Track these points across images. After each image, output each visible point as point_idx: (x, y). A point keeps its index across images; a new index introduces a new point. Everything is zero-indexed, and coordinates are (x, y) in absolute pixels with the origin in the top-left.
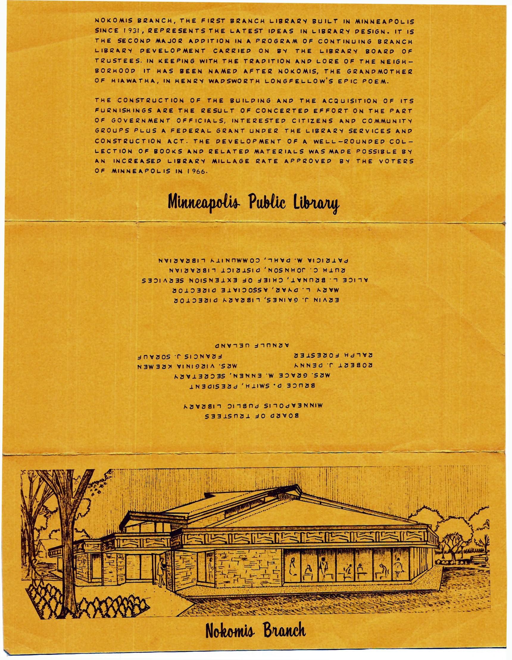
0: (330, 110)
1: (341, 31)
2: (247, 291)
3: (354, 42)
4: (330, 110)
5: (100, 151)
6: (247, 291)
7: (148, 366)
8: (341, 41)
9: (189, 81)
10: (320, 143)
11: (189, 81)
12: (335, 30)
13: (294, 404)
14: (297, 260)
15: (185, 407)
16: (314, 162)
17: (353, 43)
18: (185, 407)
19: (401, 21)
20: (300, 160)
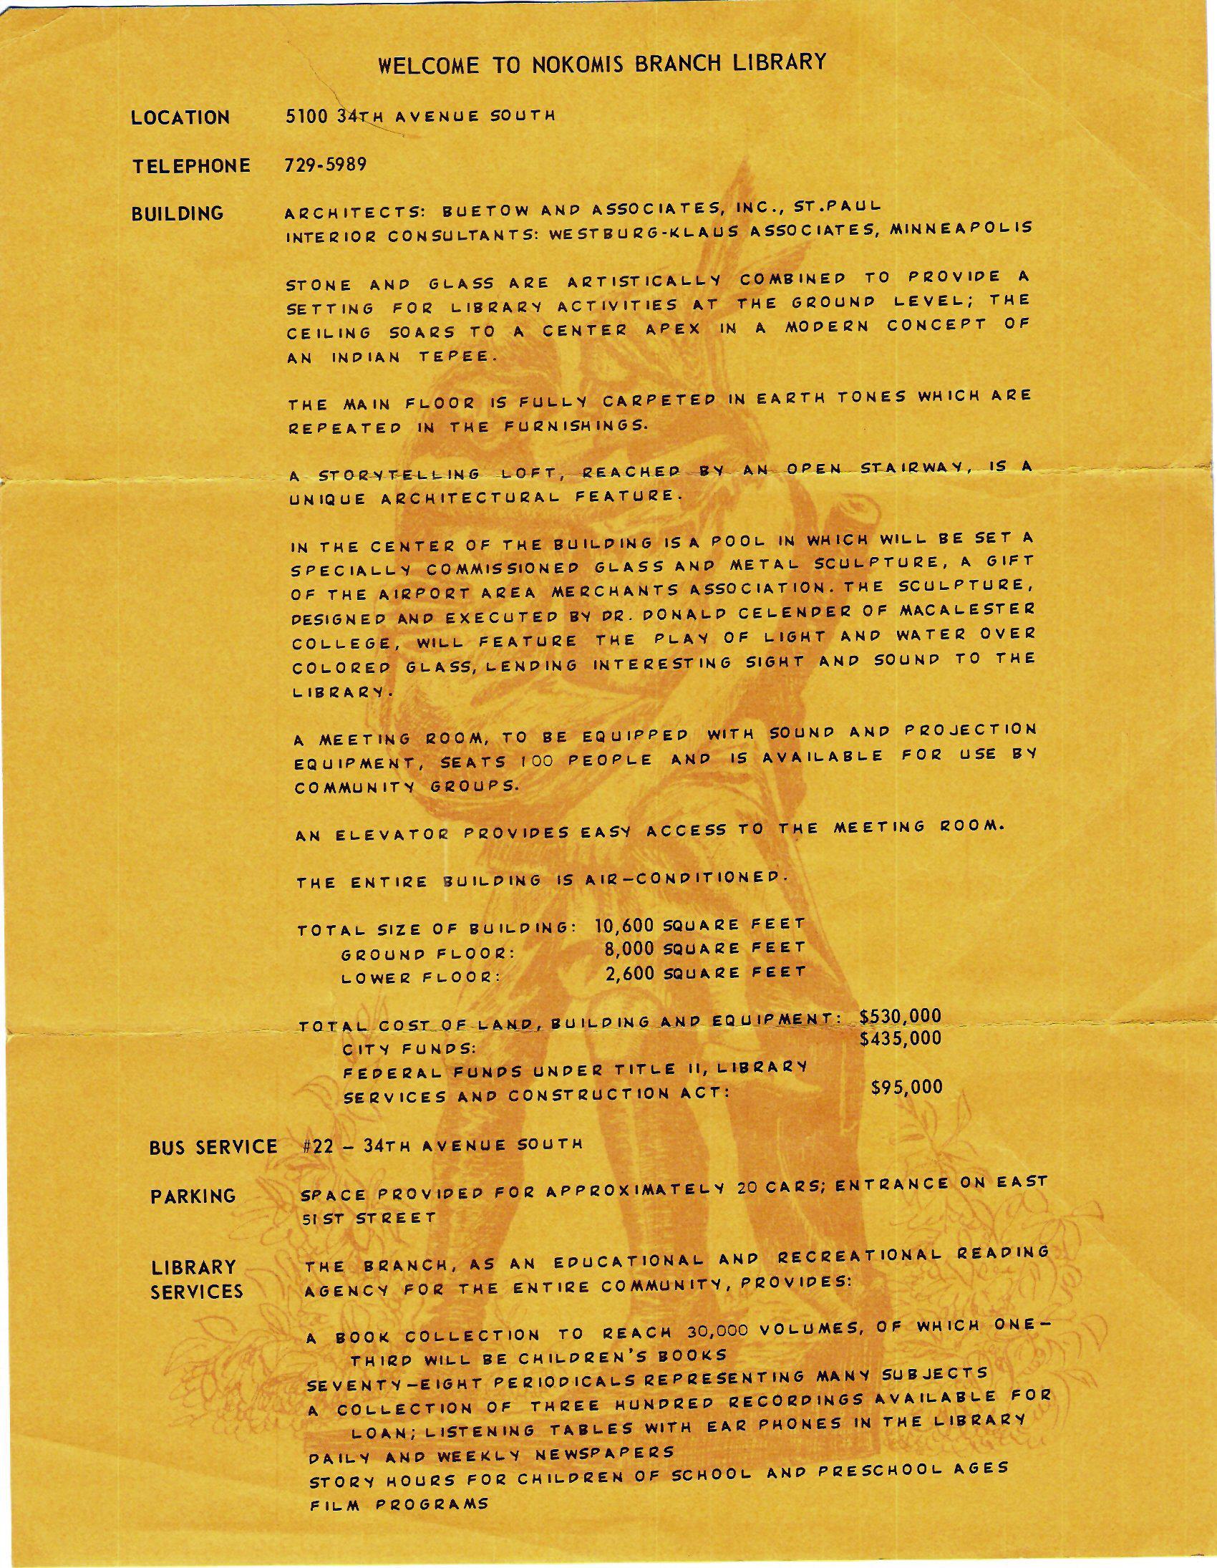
0: (404, 307)
1: (799, 1185)
2: (799, 229)
3: (345, 500)
4: (404, 307)
5: (462, 1337)
6: (799, 229)
7: (744, 567)
8: (768, 1377)
9: (922, 326)
10: (388, 982)
11: (922, 326)
12: (453, 1501)
13: (944, 614)
14: (998, 826)
15: (370, 1482)
16: (994, 635)
17: (456, 120)
18: (370, 1482)
19: (703, 612)
20: (917, 273)
